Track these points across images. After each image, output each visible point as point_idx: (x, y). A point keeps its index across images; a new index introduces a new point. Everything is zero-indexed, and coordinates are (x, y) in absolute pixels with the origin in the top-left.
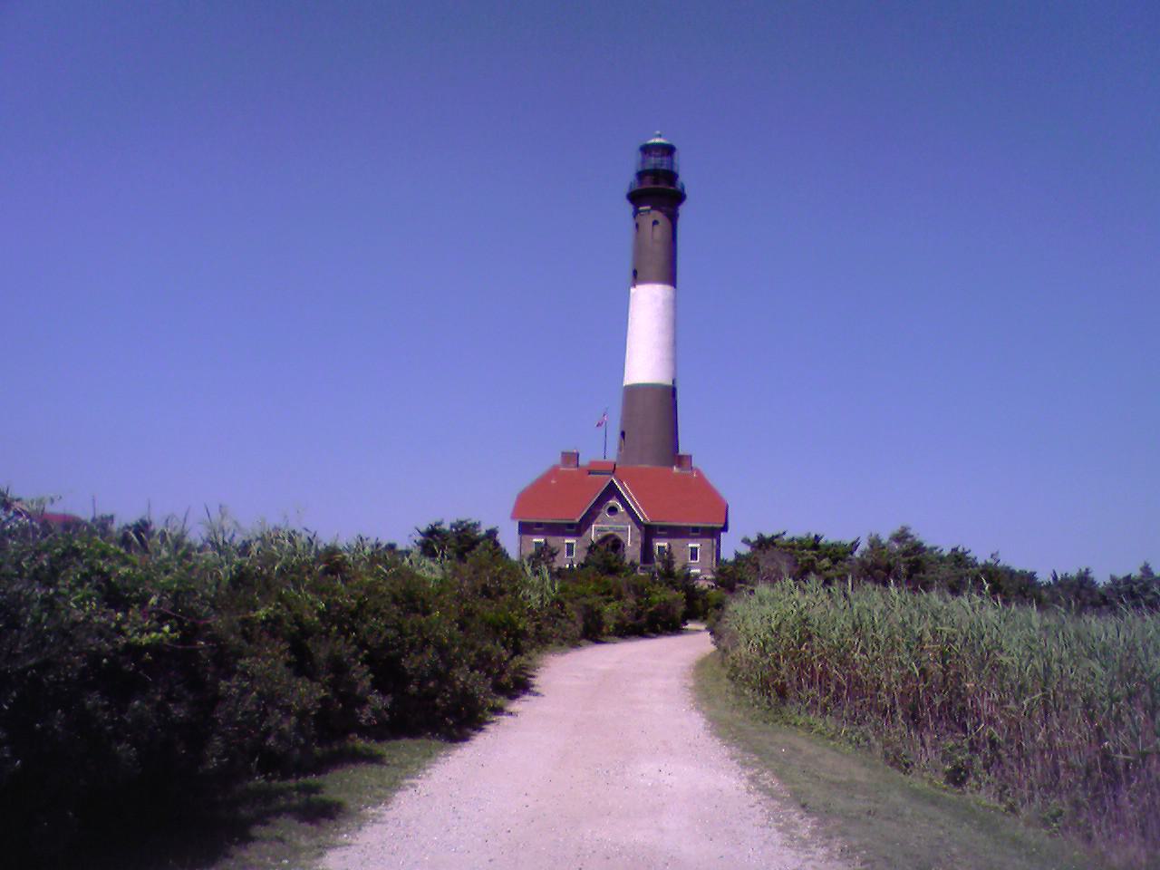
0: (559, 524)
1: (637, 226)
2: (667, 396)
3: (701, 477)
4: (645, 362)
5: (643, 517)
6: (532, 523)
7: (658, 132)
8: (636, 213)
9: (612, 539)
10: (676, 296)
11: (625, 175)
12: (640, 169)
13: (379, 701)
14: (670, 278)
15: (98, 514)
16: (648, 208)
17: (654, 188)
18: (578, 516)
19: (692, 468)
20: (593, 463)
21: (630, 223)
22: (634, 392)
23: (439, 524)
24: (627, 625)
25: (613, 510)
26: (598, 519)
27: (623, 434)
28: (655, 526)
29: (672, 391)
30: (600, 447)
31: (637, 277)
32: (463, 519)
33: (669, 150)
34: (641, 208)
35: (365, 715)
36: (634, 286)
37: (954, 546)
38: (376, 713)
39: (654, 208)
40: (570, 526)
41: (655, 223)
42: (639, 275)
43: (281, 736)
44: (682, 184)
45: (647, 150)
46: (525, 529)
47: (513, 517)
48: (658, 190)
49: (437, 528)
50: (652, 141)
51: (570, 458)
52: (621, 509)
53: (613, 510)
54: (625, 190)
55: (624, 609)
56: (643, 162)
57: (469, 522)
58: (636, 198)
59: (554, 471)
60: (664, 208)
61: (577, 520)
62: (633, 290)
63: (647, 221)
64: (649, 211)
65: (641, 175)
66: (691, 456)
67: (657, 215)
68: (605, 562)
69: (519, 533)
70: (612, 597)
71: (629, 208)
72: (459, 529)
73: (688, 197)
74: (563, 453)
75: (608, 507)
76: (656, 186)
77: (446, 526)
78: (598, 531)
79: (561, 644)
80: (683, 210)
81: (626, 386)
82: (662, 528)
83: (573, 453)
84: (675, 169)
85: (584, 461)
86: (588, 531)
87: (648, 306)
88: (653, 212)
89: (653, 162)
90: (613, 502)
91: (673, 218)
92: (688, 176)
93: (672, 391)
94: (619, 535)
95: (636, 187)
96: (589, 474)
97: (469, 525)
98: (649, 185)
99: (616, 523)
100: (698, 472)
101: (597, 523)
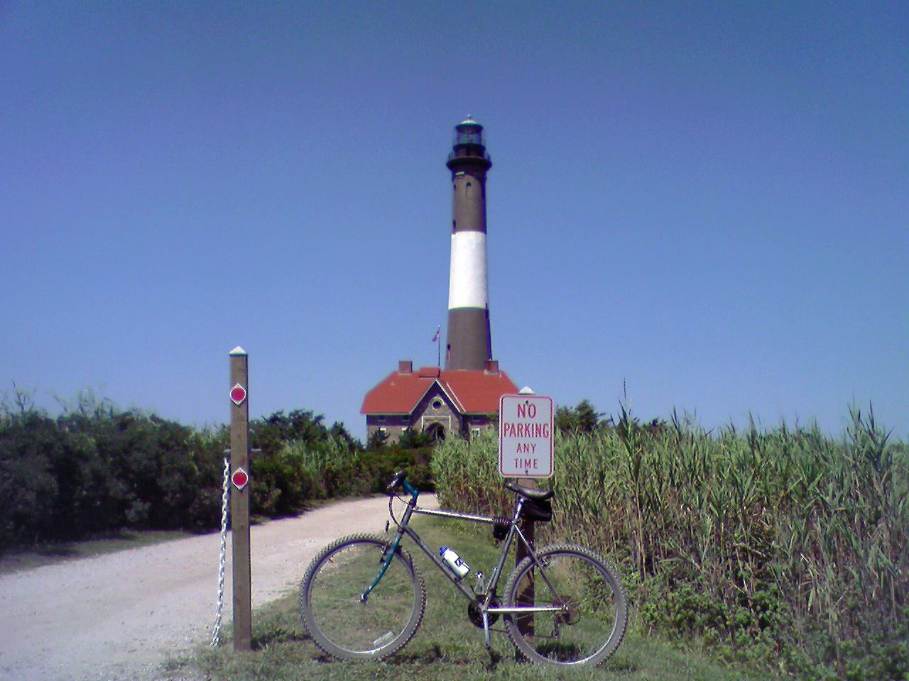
0: (400, 416)
1: (455, 186)
2: (483, 316)
3: (505, 377)
4: (464, 290)
5: (461, 408)
6: (376, 416)
7: (469, 115)
8: (454, 177)
9: (438, 427)
10: (486, 241)
11: (446, 151)
12: (456, 144)
13: (140, 506)
14: (482, 226)
15: (33, 410)
16: (463, 173)
17: (467, 159)
18: (411, 410)
19: (498, 371)
20: (422, 369)
21: (450, 185)
22: (456, 314)
23: (281, 413)
24: (419, 484)
25: (437, 405)
26: (426, 412)
27: (449, 347)
28: (470, 416)
29: (486, 313)
30: (430, 357)
31: (456, 227)
32: (298, 408)
33: (477, 129)
34: (457, 174)
35: (131, 515)
36: (454, 233)
37: (654, 417)
38: (138, 513)
39: (467, 173)
40: (406, 417)
41: (469, 184)
42: (457, 225)
43: (27, 503)
44: (488, 155)
45: (461, 129)
46: (371, 420)
47: (363, 411)
48: (470, 160)
49: (279, 416)
50: (465, 122)
51: (407, 365)
52: (444, 403)
53: (437, 405)
54: (446, 160)
55: (416, 472)
56: (458, 138)
57: (304, 411)
58: (453, 166)
59: (393, 376)
60: (475, 173)
61: (410, 413)
62: (453, 236)
63: (462, 183)
64: (463, 175)
65: (457, 148)
66: (497, 362)
67: (470, 179)
68: (411, 439)
69: (367, 424)
70: (408, 463)
71: (449, 173)
72: (297, 417)
73: (445, 164)
74: (400, 363)
75: (433, 403)
76: (469, 157)
77: (286, 415)
78: (426, 420)
79: (358, 496)
80: (490, 174)
81: (450, 311)
82: (476, 417)
83: (407, 362)
84: (483, 144)
85: (416, 368)
86: (418, 422)
87: (465, 245)
88: (466, 176)
89: (465, 139)
90: (438, 398)
91: (482, 181)
92: (492, 151)
93: (486, 313)
94: (442, 423)
95: (454, 157)
96: (420, 377)
97: (303, 414)
98: (463, 156)
99: (439, 415)
100: (503, 374)
101: (426, 415)
